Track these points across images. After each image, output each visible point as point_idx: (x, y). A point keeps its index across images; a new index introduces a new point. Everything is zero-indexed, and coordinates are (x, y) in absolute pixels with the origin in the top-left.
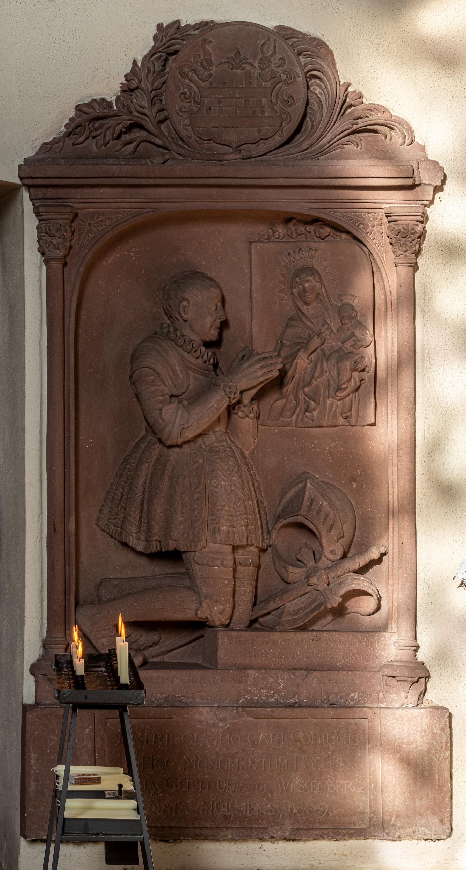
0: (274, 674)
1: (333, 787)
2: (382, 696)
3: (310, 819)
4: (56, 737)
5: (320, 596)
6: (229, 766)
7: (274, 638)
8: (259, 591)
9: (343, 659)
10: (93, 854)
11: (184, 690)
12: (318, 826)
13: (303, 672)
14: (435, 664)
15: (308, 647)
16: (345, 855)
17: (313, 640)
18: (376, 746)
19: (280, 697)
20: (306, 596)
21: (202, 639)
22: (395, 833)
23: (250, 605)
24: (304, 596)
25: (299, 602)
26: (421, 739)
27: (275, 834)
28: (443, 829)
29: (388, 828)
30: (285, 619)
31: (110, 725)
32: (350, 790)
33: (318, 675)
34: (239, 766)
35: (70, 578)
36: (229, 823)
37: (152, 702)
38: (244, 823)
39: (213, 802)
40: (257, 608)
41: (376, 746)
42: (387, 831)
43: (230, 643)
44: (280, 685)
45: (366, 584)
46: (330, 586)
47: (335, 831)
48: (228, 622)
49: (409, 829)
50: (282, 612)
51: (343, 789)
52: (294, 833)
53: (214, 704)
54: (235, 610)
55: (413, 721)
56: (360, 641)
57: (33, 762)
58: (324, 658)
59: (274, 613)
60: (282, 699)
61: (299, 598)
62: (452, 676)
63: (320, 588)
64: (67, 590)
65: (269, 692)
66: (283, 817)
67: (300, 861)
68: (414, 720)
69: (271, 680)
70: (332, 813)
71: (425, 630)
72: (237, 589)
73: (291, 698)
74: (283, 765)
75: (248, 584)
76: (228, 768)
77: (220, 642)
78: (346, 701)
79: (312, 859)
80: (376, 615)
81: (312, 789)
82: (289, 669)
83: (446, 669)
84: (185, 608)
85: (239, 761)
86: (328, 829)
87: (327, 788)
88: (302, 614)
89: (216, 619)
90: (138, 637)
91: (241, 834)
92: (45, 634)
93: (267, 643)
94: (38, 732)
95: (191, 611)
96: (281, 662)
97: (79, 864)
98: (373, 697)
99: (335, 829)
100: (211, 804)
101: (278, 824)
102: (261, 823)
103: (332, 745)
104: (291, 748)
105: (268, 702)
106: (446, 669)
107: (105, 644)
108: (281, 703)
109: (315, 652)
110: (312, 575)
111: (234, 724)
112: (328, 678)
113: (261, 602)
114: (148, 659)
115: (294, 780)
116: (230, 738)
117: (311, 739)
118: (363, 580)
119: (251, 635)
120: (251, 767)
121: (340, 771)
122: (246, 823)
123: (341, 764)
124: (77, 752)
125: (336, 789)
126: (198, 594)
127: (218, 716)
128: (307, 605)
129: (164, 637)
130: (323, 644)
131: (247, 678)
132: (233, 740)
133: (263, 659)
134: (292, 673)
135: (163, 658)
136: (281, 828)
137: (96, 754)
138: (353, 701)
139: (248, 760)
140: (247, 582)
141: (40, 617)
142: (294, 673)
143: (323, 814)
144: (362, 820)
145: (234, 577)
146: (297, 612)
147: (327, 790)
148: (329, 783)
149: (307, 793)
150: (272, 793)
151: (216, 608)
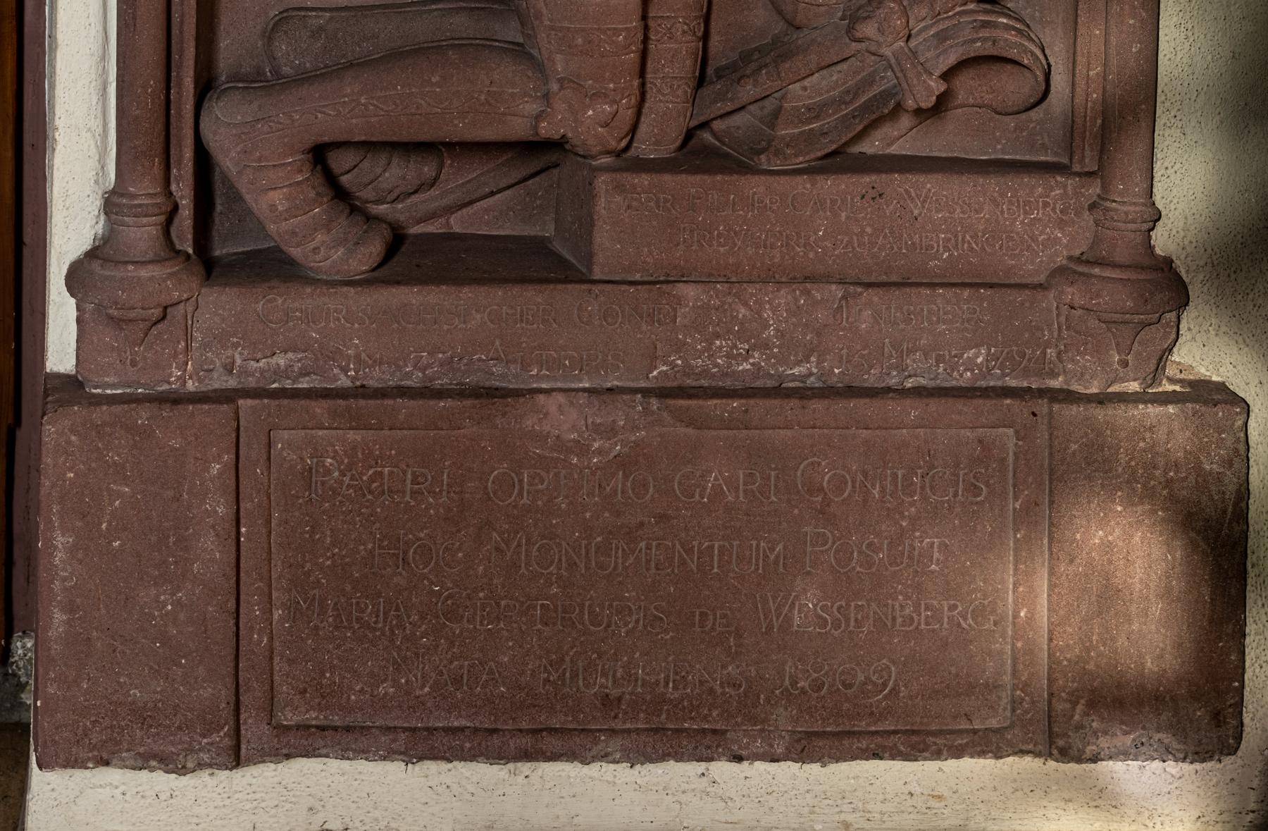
0: (752, 295)
1: (912, 619)
2: (1054, 358)
3: (846, 706)
4: (127, 485)
5: (885, 70)
6: (620, 561)
7: (755, 193)
8: (715, 40)
9: (946, 249)
10: (236, 792)
11: (497, 343)
12: (868, 725)
13: (834, 287)
14: (1202, 263)
15: (848, 218)
16: (940, 797)
17: (863, 197)
18: (1037, 504)
19: (768, 359)
20: (844, 66)
21: (555, 171)
22: (1085, 747)
23: (684, 89)
24: (839, 67)
25: (824, 83)
26: (1164, 488)
27: (747, 748)
28: (1219, 737)
29: (1066, 735)
30: (785, 131)
31: (283, 448)
32: (959, 625)
33: (876, 299)
34: (648, 562)
35: (182, 23)
36: (616, 717)
37: (407, 373)
38: (659, 716)
39: (572, 661)
40: (706, 91)
41: (1037, 504)
42: (1061, 743)
43: (629, 207)
44: (767, 327)
45: (1014, 39)
46: (912, 44)
47: (915, 738)
48: (624, 144)
49: (1122, 738)
50: (777, 113)
51: (940, 621)
52: (799, 747)
53: (581, 381)
54: (647, 105)
55: (1144, 440)
56: (994, 201)
57: (59, 557)
58: (892, 248)
59: (752, 108)
60: (774, 365)
61: (825, 72)
62: (1251, 296)
63: (887, 52)
64: (175, 57)
65: (735, 346)
66: (768, 701)
67: (812, 813)
68: (1148, 435)
69: (743, 312)
70: (906, 686)
71: (1177, 166)
72: (652, 47)
73: (798, 363)
74: (772, 557)
75: (684, 32)
76: (615, 568)
77: (602, 202)
78: (953, 370)
79: (846, 808)
80: (1035, 114)
81: (852, 623)
82: (793, 280)
83: (1233, 276)
84: (504, 114)
85: (648, 548)
86: (895, 732)
87: (894, 619)
88: (830, 120)
89: (591, 141)
90: (379, 171)
91: (649, 750)
92: (113, 176)
93: (734, 204)
94: (76, 474)
95: (520, 120)
96: (771, 259)
97: (195, 820)
98: (1030, 360)
99: (913, 732)
100: (567, 664)
101: (753, 720)
102: (705, 717)
103: (913, 504)
104: (796, 511)
105: (734, 372)
106: (1233, 276)
107: (280, 208)
108: (769, 374)
109: (869, 230)
110: (862, 13)
111: (637, 444)
112: (905, 308)
113: (720, 74)
114: (404, 228)
115: (803, 597)
116: (624, 485)
117: (853, 487)
118: (1007, 27)
119: (691, 184)
120: (683, 563)
121: (933, 572)
122: (664, 716)
123: (936, 555)
124: (187, 529)
125: (919, 624)
126: (539, 67)
127: (590, 421)
128: (848, 92)
129: (451, 166)
130: (891, 207)
131: (675, 310)
132: (633, 490)
133: (722, 249)
134: (801, 292)
135: (448, 223)
136: (762, 730)
137: (243, 530)
138: (972, 371)
139: (674, 546)
140: (681, 27)
141: (100, 129)
142: (807, 293)
143: (881, 692)
144: (992, 707)
145: (644, 17)
146: (816, 112)
147: (894, 625)
148: (901, 606)
149: (836, 633)
150: (739, 636)
151: (590, 112)
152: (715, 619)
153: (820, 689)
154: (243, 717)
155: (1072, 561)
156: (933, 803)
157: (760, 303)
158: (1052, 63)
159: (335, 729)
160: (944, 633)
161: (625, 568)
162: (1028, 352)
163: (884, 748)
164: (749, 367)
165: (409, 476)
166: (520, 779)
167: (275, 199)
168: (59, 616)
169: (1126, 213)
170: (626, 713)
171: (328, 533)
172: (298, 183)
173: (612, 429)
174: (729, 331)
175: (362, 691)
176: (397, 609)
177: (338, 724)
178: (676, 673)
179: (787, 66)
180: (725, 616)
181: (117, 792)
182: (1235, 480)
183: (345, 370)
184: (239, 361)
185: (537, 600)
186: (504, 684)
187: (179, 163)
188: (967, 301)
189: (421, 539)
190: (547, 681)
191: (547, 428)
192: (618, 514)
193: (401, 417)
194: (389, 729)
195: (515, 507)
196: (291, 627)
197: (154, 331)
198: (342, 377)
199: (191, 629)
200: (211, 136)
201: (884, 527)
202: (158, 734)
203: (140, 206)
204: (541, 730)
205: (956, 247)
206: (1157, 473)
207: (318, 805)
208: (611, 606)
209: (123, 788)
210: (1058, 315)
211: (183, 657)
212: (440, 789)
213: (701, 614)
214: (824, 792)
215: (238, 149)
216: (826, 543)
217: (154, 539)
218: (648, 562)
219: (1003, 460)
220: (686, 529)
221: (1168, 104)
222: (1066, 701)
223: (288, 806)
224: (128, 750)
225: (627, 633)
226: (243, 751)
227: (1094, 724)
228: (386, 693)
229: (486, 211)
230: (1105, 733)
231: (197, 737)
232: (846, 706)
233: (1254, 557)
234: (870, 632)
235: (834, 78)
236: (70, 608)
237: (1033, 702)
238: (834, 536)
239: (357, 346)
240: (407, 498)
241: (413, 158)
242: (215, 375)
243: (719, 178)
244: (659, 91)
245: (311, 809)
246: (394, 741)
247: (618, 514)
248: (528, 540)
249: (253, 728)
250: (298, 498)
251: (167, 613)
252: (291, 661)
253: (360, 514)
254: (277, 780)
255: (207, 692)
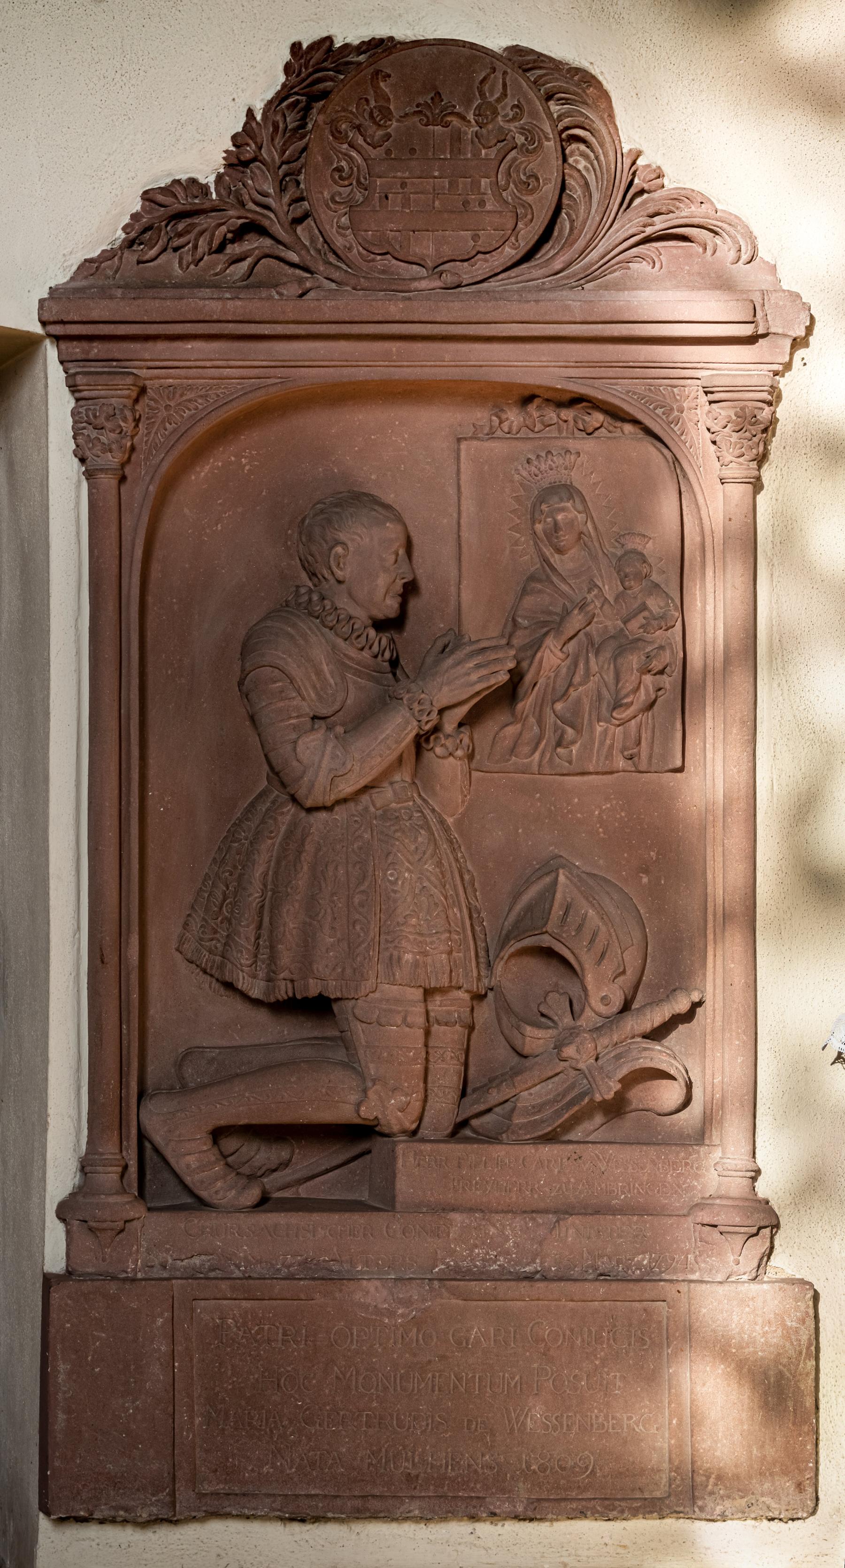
0: (498, 1220)
1: (603, 1425)
2: (693, 1261)
4: (104, 1332)
5: (582, 1080)
6: (416, 1385)
8: (472, 1070)
9: (623, 1193)
10: (170, 1544)
11: (335, 1250)
12: (577, 1495)
13: (551, 1216)
14: (788, 1203)
15: (559, 1172)
16: (625, 1547)
17: (569, 1159)
20: (556, 1079)
21: (368, 1157)
24: (553, 1080)
27: (499, 1508)
28: (801, 1500)
30: (518, 1120)
31: (201, 1312)
32: (634, 1429)
34: (433, 1386)
35: (129, 1046)
36: (415, 1488)
37: (278, 1270)
46: (600, 1062)
47: (607, 1502)
48: (414, 1126)
49: (739, 1501)
50: (513, 1110)
52: (533, 1507)
53: (389, 1274)
54: (428, 1104)
56: (653, 1161)
57: (61, 1378)
60: (513, 1265)
61: (544, 1084)
63: (581, 1066)
64: (125, 1069)
65: (488, 1253)
66: (512, 1478)
67: (543, 1557)
68: (751, 1303)
69: (492, 1231)
72: (431, 1066)
73: (528, 1264)
74: (513, 1384)
75: (452, 1058)
76: (413, 1390)
82: (525, 1212)
83: (809, 1211)
84: (338, 1102)
85: (434, 1377)
87: (592, 1425)
88: (548, 1112)
89: (393, 1121)
90: (252, 1153)
91: (437, 1508)
92: (84, 1147)
93: (485, 1163)
94: (72, 1325)
95: (348, 1106)
96: (510, 1198)
97: (144, 1562)
98: (677, 1262)
99: (606, 1499)
101: (503, 1491)
102: (472, 1488)
103: (603, 1349)
105: (487, 1271)
106: (809, 1211)
107: (193, 1166)
108: (510, 1272)
109: (572, 1180)
110: (566, 1042)
111: (426, 1310)
115: (533, 1410)
117: (564, 1338)
120: (455, 1387)
121: (616, 1395)
122: (446, 1488)
123: (618, 1383)
128: (559, 1095)
129: (299, 1153)
133: (478, 1193)
135: (297, 1192)
136: (509, 1497)
137: (176, 1364)
138: (640, 1270)
139: (450, 1375)
140: (449, 1054)
141: (76, 1117)
142: (534, 1219)
143: (585, 1472)
144: (656, 1484)
145: (426, 1045)
146: (539, 1108)
147: (591, 1430)
150: (493, 1435)
151: (393, 1101)
152: (477, 1424)
153: (545, 1470)
154: (177, 1486)
155: (704, 1385)
156: (620, 1550)
157: (504, 1226)
158: (693, 1080)
159: (236, 1495)
160: (625, 1434)
161: (419, 1390)
162: (676, 1257)
163: (587, 1508)
164: (497, 1267)
165: (281, 1331)
166: (354, 1537)
167: (192, 1157)
168: (61, 1416)
169: (736, 1165)
170: (421, 1486)
171: (229, 1367)
172: (205, 1151)
173: (410, 1301)
174: (483, 1243)
175: (252, 1470)
176: (274, 1418)
177: (237, 1492)
178: (453, 1459)
179: (519, 1078)
180: (483, 1422)
181: (94, 1544)
182: (807, 1332)
183: (238, 1267)
184: (170, 1261)
185: (364, 1411)
186: (343, 1466)
187: (128, 1138)
188: (636, 1223)
189: (288, 1371)
190: (370, 1464)
191: (369, 1300)
192: (415, 1355)
193: (276, 1291)
194: (270, 1495)
195: (349, 1350)
196: (207, 1429)
197: (117, 1239)
198: (237, 1271)
199: (144, 1425)
200: (147, 1122)
201: (584, 1365)
202: (124, 1493)
203: (107, 1159)
204: (367, 1496)
205: (629, 1191)
206: (758, 1328)
207: (223, 1553)
208: (410, 1415)
209: (97, 1541)
210: (694, 1231)
211: (140, 1443)
212: (302, 1543)
213: (468, 1420)
214: (550, 1544)
215: (165, 1129)
216: (547, 1375)
217: (121, 1367)
218: (433, 1386)
219: (660, 1322)
220: (458, 1365)
221: (764, 1100)
222: (703, 1475)
223: (204, 1553)
224: (106, 1504)
225: (422, 1432)
226: (178, 1508)
227: (721, 1492)
228: (268, 1472)
229: (323, 1183)
230: (729, 1497)
231: (149, 1496)
232: (562, 1482)
233: (825, 1391)
234: (577, 1434)
235: (550, 1087)
236: (68, 1411)
237: (682, 1479)
238: (552, 1370)
239: (245, 1251)
240: (280, 1345)
241: (274, 1147)
242: (155, 1270)
243: (475, 1146)
244: (436, 1095)
245: (219, 1555)
246: (274, 1502)
247: (415, 1355)
248: (358, 1373)
249: (184, 1496)
250: (211, 1344)
251: (130, 1415)
252: (207, 1451)
253: (250, 1355)
254: (197, 1536)
255: (155, 1466)
